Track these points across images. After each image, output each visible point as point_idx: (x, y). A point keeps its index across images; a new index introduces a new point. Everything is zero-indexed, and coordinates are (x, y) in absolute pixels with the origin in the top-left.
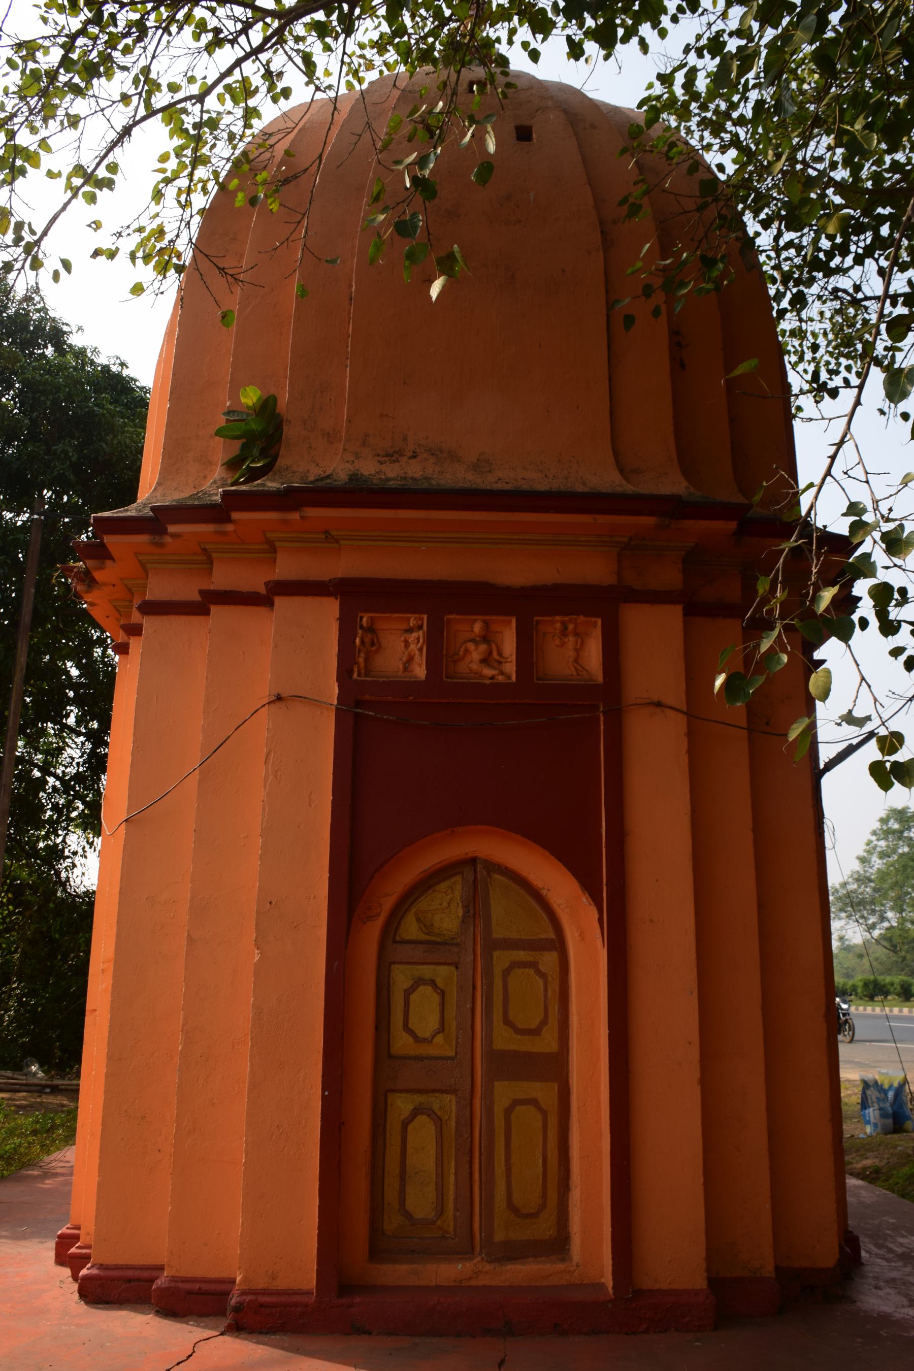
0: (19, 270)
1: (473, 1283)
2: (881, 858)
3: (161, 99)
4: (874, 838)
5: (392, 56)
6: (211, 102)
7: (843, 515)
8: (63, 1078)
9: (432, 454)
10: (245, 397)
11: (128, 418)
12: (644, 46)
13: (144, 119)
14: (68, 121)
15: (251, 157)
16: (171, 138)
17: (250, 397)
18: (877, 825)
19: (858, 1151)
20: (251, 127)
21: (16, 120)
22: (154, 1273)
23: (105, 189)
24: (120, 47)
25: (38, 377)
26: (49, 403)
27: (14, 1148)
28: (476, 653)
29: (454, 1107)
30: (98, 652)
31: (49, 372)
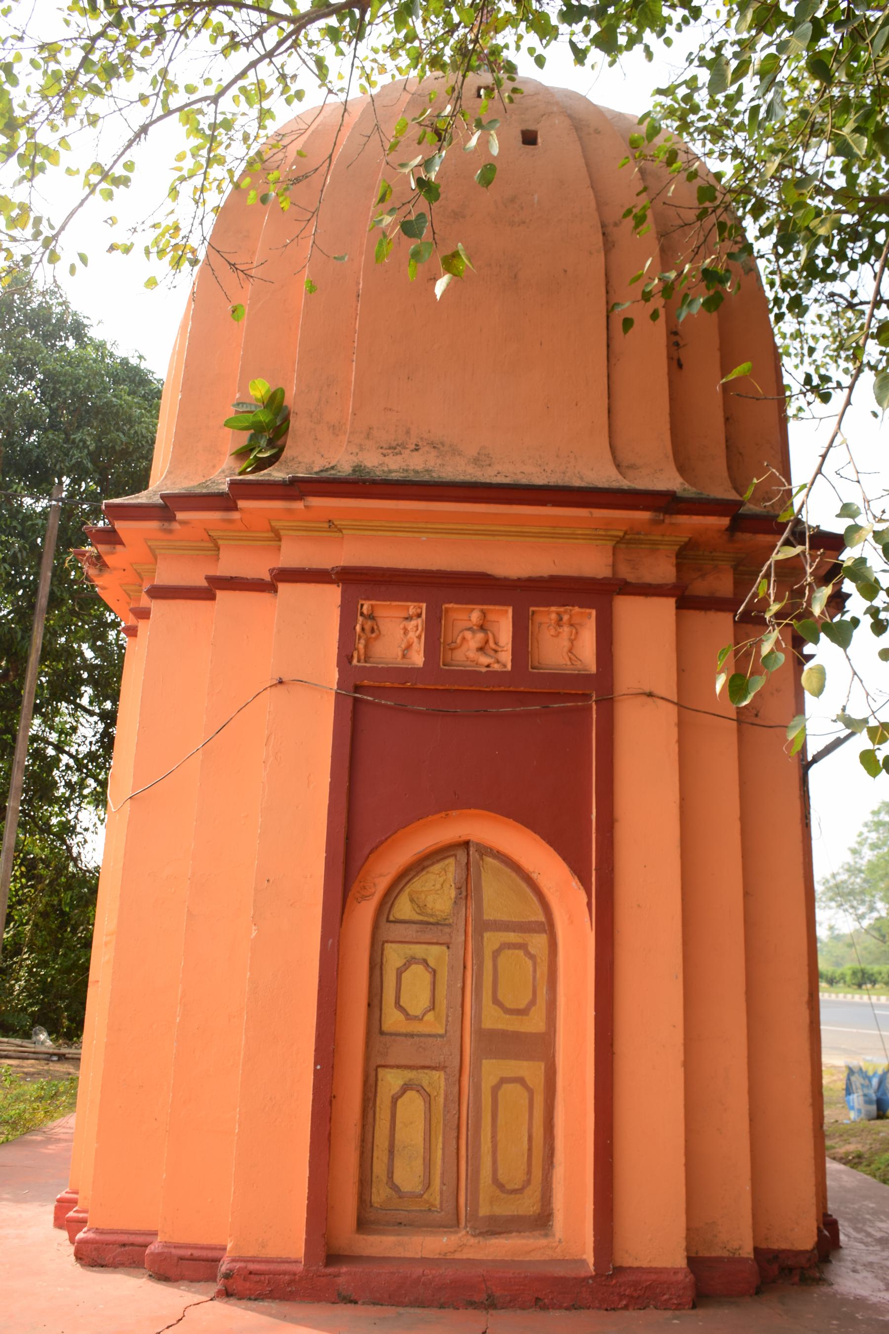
0: (38, 263)
1: (457, 1256)
2: (872, 850)
3: (177, 100)
4: (865, 830)
5: (404, 60)
6: (225, 103)
7: (838, 516)
8: (70, 1047)
9: (434, 447)
10: (254, 389)
11: (145, 409)
12: (649, 54)
13: (160, 118)
14: (88, 119)
15: (265, 157)
16: (188, 138)
17: (259, 389)
18: (869, 818)
19: (841, 1136)
20: (265, 128)
21: (36, 119)
22: (148, 1239)
23: (121, 187)
24: (140, 48)
25: (58, 368)
26: (68, 393)
27: (19, 1114)
28: (474, 641)
29: (443, 1083)
30: (112, 635)
31: (70, 364)
